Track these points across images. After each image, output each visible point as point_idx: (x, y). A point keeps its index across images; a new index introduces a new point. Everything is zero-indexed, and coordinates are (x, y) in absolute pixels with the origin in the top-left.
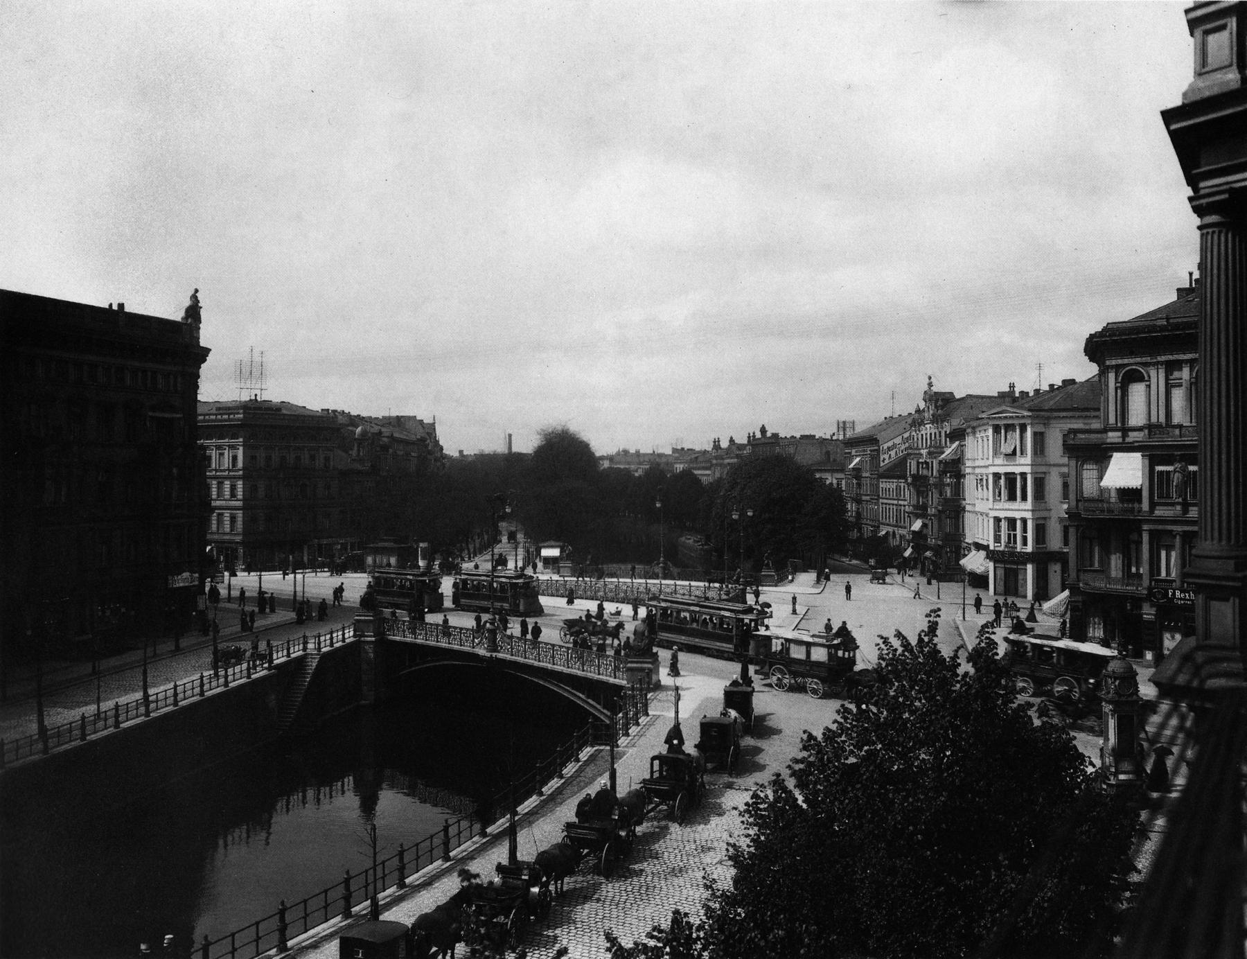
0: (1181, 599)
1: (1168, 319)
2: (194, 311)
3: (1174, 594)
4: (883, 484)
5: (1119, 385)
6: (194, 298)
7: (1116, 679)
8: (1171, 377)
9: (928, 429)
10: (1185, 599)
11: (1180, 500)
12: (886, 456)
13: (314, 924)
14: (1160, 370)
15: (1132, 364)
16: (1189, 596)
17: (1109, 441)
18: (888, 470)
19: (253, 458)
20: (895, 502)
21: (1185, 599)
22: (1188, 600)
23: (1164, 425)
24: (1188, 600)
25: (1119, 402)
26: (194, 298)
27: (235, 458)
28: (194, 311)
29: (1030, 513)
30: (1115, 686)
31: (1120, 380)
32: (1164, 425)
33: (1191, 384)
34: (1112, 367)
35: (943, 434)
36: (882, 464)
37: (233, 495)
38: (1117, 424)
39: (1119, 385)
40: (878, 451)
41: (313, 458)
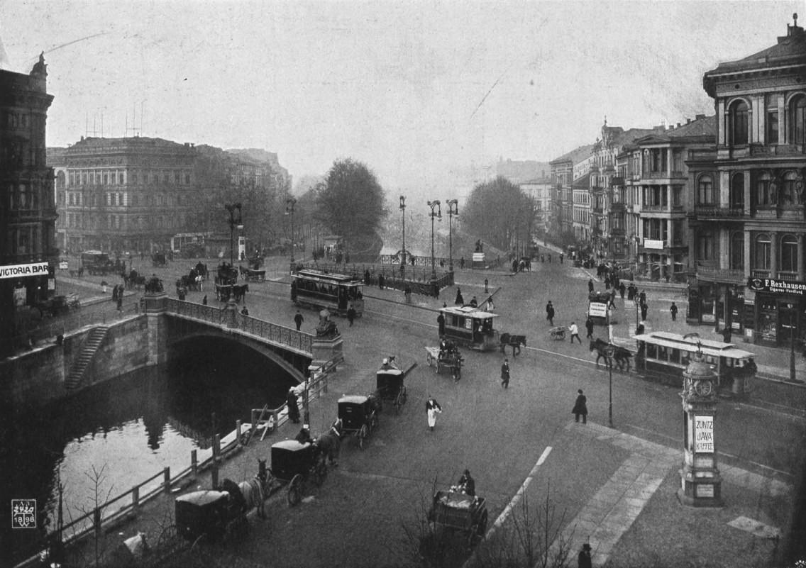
0: (776, 288)
1: (767, 57)
2: (40, 68)
3: (770, 283)
4: (575, 192)
5: (727, 113)
6: (41, 57)
7: (694, 380)
8: (770, 106)
9: (604, 153)
10: (778, 288)
11: (775, 206)
12: (578, 174)
13: (598, 319)
14: (760, 100)
15: (738, 96)
16: (782, 285)
17: (719, 158)
18: (579, 183)
19: (134, 176)
20: (583, 206)
21: (778, 288)
22: (781, 288)
23: (763, 144)
24: (781, 288)
25: (727, 123)
26: (41, 57)
27: (121, 176)
28: (40, 68)
29: (670, 215)
30: (694, 388)
31: (728, 109)
32: (763, 144)
33: (785, 111)
34: (722, 98)
35: (614, 157)
36: (574, 179)
37: (121, 204)
38: (725, 145)
39: (750, 111)
40: (572, 169)
41: (177, 177)
